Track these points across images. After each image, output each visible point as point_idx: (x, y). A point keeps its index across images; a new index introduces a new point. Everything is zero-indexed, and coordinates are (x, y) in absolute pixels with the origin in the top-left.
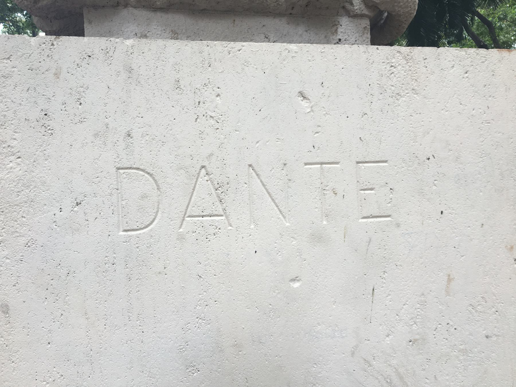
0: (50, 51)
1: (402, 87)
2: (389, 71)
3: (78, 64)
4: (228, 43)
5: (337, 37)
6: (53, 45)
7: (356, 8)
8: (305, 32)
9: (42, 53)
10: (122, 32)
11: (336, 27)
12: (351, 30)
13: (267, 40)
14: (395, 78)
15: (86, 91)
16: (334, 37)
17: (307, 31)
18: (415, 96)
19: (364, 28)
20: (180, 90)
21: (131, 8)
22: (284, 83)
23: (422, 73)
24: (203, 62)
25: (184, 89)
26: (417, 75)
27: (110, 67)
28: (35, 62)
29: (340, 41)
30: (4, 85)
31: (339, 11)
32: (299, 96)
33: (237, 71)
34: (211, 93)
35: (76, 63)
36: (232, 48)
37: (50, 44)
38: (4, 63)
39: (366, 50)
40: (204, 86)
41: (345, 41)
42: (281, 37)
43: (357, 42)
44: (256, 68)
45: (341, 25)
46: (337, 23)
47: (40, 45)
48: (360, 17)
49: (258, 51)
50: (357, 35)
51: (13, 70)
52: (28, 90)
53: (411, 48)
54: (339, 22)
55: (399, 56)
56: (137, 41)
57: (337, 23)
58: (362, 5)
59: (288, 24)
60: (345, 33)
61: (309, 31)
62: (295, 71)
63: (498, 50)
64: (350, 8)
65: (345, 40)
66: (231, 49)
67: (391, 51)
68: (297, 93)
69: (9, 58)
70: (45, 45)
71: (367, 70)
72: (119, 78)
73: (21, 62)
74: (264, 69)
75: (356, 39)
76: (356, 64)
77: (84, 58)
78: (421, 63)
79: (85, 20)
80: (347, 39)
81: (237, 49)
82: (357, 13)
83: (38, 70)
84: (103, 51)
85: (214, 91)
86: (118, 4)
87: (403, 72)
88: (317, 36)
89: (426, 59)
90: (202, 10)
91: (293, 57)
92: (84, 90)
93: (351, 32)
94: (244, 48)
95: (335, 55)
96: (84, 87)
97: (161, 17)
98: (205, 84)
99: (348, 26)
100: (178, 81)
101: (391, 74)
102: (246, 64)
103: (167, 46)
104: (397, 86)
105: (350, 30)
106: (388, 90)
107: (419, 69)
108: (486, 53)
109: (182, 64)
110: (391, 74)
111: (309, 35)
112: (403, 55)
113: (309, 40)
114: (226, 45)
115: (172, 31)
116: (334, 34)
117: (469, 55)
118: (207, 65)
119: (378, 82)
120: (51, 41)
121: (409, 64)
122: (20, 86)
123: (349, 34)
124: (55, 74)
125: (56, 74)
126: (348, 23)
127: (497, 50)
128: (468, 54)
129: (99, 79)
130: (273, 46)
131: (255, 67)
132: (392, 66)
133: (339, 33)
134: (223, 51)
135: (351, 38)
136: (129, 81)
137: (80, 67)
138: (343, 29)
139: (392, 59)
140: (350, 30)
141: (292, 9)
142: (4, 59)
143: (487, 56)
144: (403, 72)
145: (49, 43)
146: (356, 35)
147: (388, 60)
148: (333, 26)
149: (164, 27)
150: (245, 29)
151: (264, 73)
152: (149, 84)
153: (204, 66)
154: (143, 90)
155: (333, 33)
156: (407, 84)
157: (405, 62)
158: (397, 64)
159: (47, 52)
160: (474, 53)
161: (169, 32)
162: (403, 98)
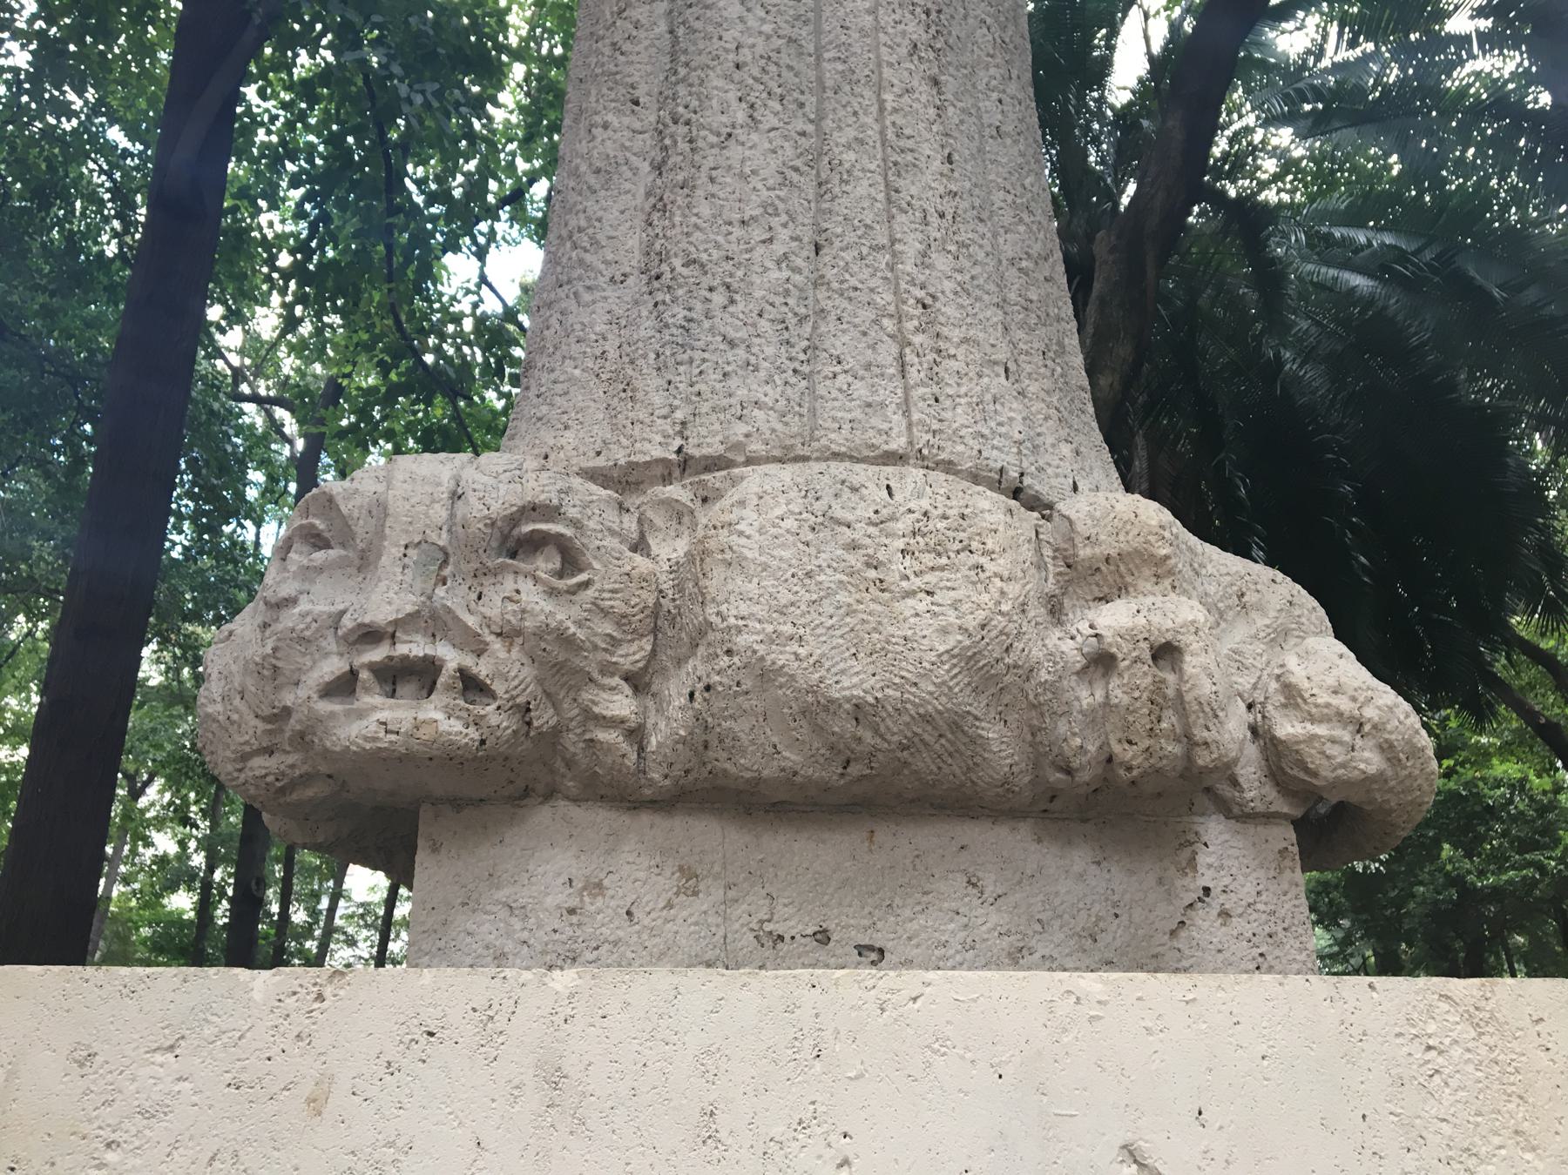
0: (307, 1021)
1: (1477, 1125)
2: (1421, 1066)
3: (389, 1063)
4: (879, 975)
6: (320, 998)
7: (1249, 795)
8: (1094, 867)
9: (282, 1029)
10: (528, 875)
11: (1189, 849)
13: (975, 891)
14: (1447, 1091)
15: (402, 1158)
16: (1186, 881)
17: (1098, 863)
18: (1528, 1156)
19: (1280, 852)
20: (717, 1148)
21: (562, 803)
22: (1069, 1112)
23: (1538, 1072)
24: (797, 1044)
25: (729, 1141)
26: (1520, 1077)
27: (493, 1071)
28: (252, 1059)
29: (1208, 895)
30: (137, 1143)
32: (1123, 1161)
33: (907, 1072)
34: (819, 1157)
35: (384, 1058)
36: (892, 991)
37: (314, 996)
38: (153, 1063)
39: (1333, 993)
40: (795, 1130)
41: (1224, 896)
42: (1020, 882)
43: (1264, 898)
44: (973, 1061)
45: (1206, 844)
47: (280, 1000)
48: (1264, 820)
49: (974, 1000)
50: (1261, 873)
51: (177, 1088)
52: (213, 1159)
53: (1483, 985)
55: (1448, 1012)
56: (588, 977)
57: (1191, 837)
59: (1039, 841)
60: (1222, 867)
61: (1105, 864)
62: (1104, 1070)
64: (1229, 795)
66: (889, 996)
67: (1417, 993)
68: (1116, 1150)
69: (171, 1048)
70: (295, 998)
71: (1348, 1063)
72: (517, 1108)
73: (209, 1061)
74: (999, 1064)
75: (1259, 888)
76: (1307, 1043)
77: (413, 1040)
78: (1525, 1035)
79: (420, 842)
80: (1231, 887)
81: (906, 994)
83: (258, 1087)
84: (477, 1014)
85: (829, 1145)
86: (527, 792)
87: (1470, 1068)
88: (1134, 878)
89: (1542, 1019)
90: (774, 804)
91: (1092, 1019)
92: (397, 1156)
93: (1240, 864)
94: (928, 989)
95: (1235, 1012)
96: (400, 1143)
97: (651, 827)
98: (799, 1124)
99: (1226, 845)
100: (712, 1114)
101: (1431, 1076)
102: (936, 1046)
103: (681, 989)
104: (1458, 1122)
105: (1237, 858)
106: (1431, 1135)
107: (1523, 1059)
109: (727, 1052)
110: (1431, 1076)
111: (1108, 877)
112: (1461, 1010)
113: (1109, 892)
114: (870, 983)
115: (681, 869)
118: (807, 1053)
119: (1391, 1107)
120: (315, 984)
121: (1486, 1039)
122: (190, 1144)
123: (1234, 871)
124: (311, 1100)
125: (314, 1101)
126: (1226, 836)
129: (450, 1113)
130: (1024, 984)
131: (968, 1055)
132: (1429, 1048)
133: (1201, 870)
134: (861, 1002)
135: (1243, 886)
136: (549, 1119)
137: (396, 1073)
139: (1425, 1022)
140: (1237, 858)
141: (1051, 801)
142: (155, 1051)
144: (1470, 1068)
145: (308, 994)
147: (1414, 1026)
149: (658, 859)
150: (905, 857)
151: (1000, 1076)
152: (615, 1127)
153: (797, 1056)
154: (592, 1149)
155: (1183, 869)
156: (1493, 1112)
157: (1473, 1034)
158: (1447, 1041)
159: (300, 1022)
161: (673, 874)
162: (1489, 1164)
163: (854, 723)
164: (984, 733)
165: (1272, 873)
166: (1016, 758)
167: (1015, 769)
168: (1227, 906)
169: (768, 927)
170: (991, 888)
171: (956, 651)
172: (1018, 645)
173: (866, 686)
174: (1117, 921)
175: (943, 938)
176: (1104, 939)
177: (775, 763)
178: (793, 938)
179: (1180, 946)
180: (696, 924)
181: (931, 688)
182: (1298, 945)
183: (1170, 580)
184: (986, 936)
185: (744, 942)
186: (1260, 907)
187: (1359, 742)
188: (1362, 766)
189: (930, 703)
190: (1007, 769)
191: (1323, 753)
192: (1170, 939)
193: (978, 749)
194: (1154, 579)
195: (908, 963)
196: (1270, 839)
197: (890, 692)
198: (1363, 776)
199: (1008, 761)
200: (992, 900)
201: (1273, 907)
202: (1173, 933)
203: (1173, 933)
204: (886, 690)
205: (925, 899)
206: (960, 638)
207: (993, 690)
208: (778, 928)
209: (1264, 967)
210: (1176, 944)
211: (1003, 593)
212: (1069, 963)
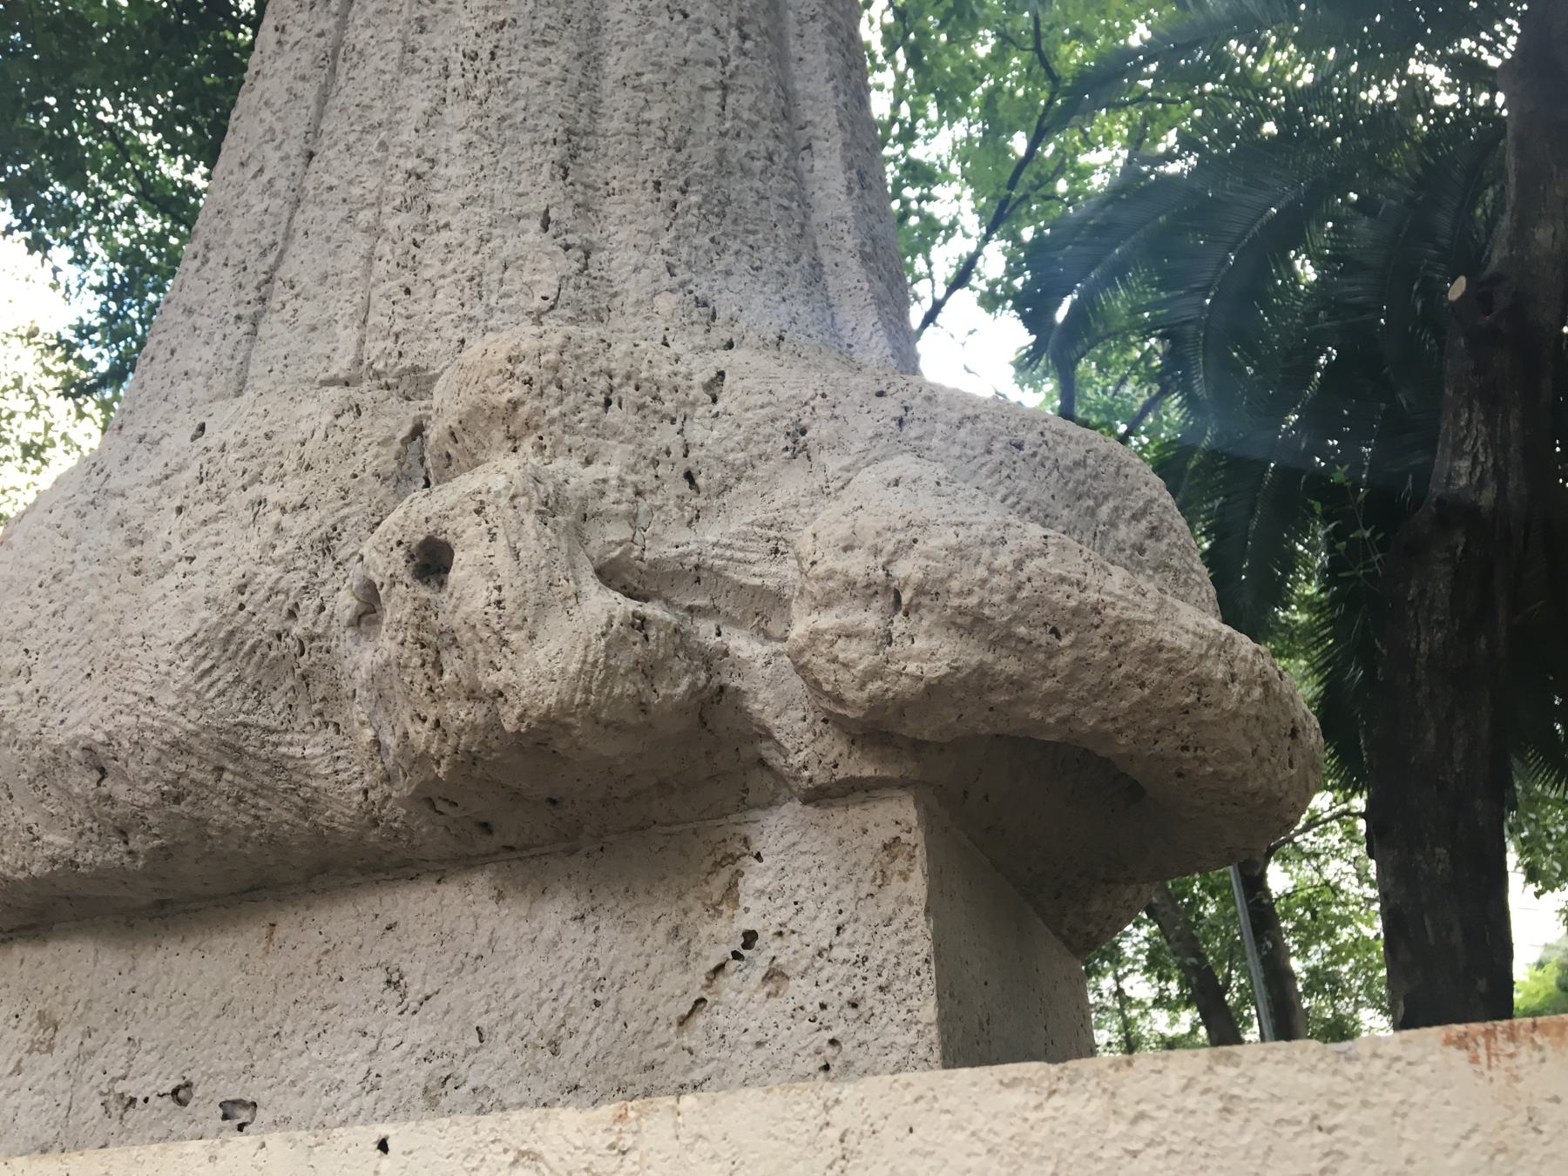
5: (735, 926)
8: (574, 926)
12: (814, 871)
19: (886, 847)
31: (749, 785)
41: (778, 942)
42: (459, 970)
43: (846, 935)
45: (758, 857)
46: (738, 845)
54: (746, 841)
57: (736, 847)
58: (827, 739)
63: (1461, 1042)
65: (780, 934)
75: (841, 918)
80: (791, 926)
82: (810, 780)
88: (633, 935)
105: (808, 871)
108: (1318, 1082)
116: (723, 907)
117: (1140, 1117)
126: (792, 837)
127: (1448, 1042)
128: (1130, 1112)
133: (745, 901)
138: (770, 873)
140: (808, 871)
143: (1340, 1118)
146: (835, 896)
148: (718, 865)
155: (714, 907)
160: (1191, 1103)
163: (96, 775)
164: (296, 751)
165: (866, 888)
166: (367, 777)
167: (372, 795)
168: (779, 961)
169: (120, 1087)
170: (417, 987)
171: (201, 635)
172: (309, 605)
173: (95, 718)
174: (596, 1014)
175: (338, 1077)
176: (570, 1046)
177: (38, 853)
178: (146, 1100)
179: (693, 1044)
180: (42, 1092)
181: (172, 700)
182: (903, 1015)
183: (533, 438)
184: (397, 1065)
185: (89, 1114)
186: (839, 953)
187: (899, 625)
188: (912, 667)
189: (175, 723)
190: (359, 798)
191: (834, 660)
192: (678, 1034)
193: (296, 777)
194: (510, 444)
195: (284, 1122)
196: (870, 826)
197: (124, 719)
198: (921, 685)
199: (357, 785)
200: (414, 1005)
201: (862, 952)
202: (683, 1021)
203: (683, 1021)
204: (118, 717)
205: (324, 1018)
206: (205, 614)
207: (290, 682)
208: (129, 1087)
209: (836, 1065)
210: (686, 1041)
211: (278, 528)
212: (512, 1096)
